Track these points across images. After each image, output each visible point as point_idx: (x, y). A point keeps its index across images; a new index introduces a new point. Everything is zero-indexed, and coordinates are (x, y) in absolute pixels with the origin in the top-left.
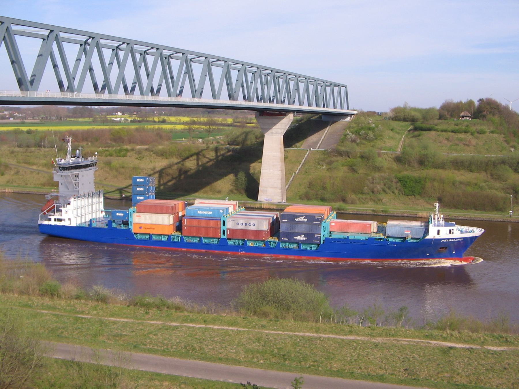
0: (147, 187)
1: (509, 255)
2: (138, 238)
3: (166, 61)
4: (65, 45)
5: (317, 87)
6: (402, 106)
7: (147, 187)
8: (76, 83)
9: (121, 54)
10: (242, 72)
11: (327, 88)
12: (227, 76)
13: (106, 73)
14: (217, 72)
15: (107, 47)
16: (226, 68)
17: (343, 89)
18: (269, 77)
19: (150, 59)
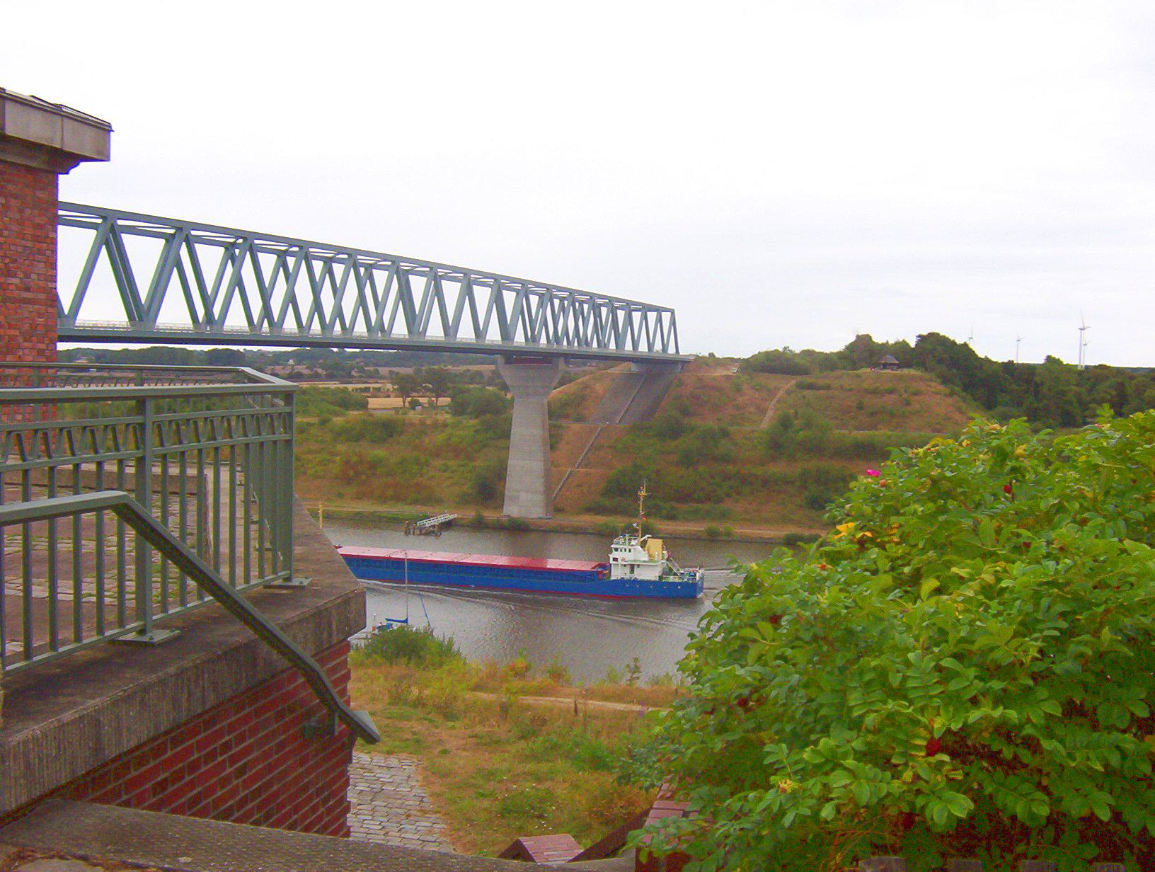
0: (978, 623)
1: (303, 665)
2: (127, 583)
3: (596, 308)
4: (199, 248)
5: (502, 294)
6: (781, 350)
7: (978, 623)
8: (217, 310)
9: (291, 261)
10: (522, 293)
11: (634, 313)
12: (498, 300)
13: (266, 295)
14: (482, 295)
15: (535, 293)
16: (465, 282)
17: (666, 317)
18: (566, 302)
19: (338, 269)
